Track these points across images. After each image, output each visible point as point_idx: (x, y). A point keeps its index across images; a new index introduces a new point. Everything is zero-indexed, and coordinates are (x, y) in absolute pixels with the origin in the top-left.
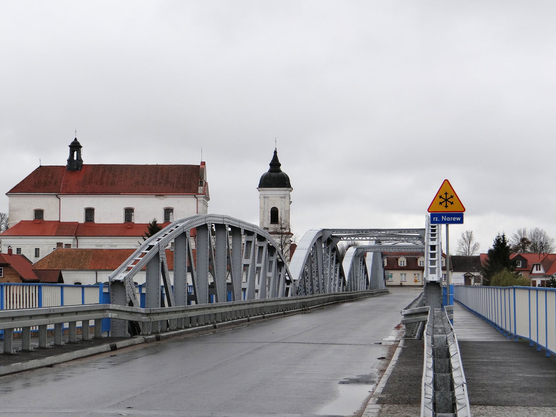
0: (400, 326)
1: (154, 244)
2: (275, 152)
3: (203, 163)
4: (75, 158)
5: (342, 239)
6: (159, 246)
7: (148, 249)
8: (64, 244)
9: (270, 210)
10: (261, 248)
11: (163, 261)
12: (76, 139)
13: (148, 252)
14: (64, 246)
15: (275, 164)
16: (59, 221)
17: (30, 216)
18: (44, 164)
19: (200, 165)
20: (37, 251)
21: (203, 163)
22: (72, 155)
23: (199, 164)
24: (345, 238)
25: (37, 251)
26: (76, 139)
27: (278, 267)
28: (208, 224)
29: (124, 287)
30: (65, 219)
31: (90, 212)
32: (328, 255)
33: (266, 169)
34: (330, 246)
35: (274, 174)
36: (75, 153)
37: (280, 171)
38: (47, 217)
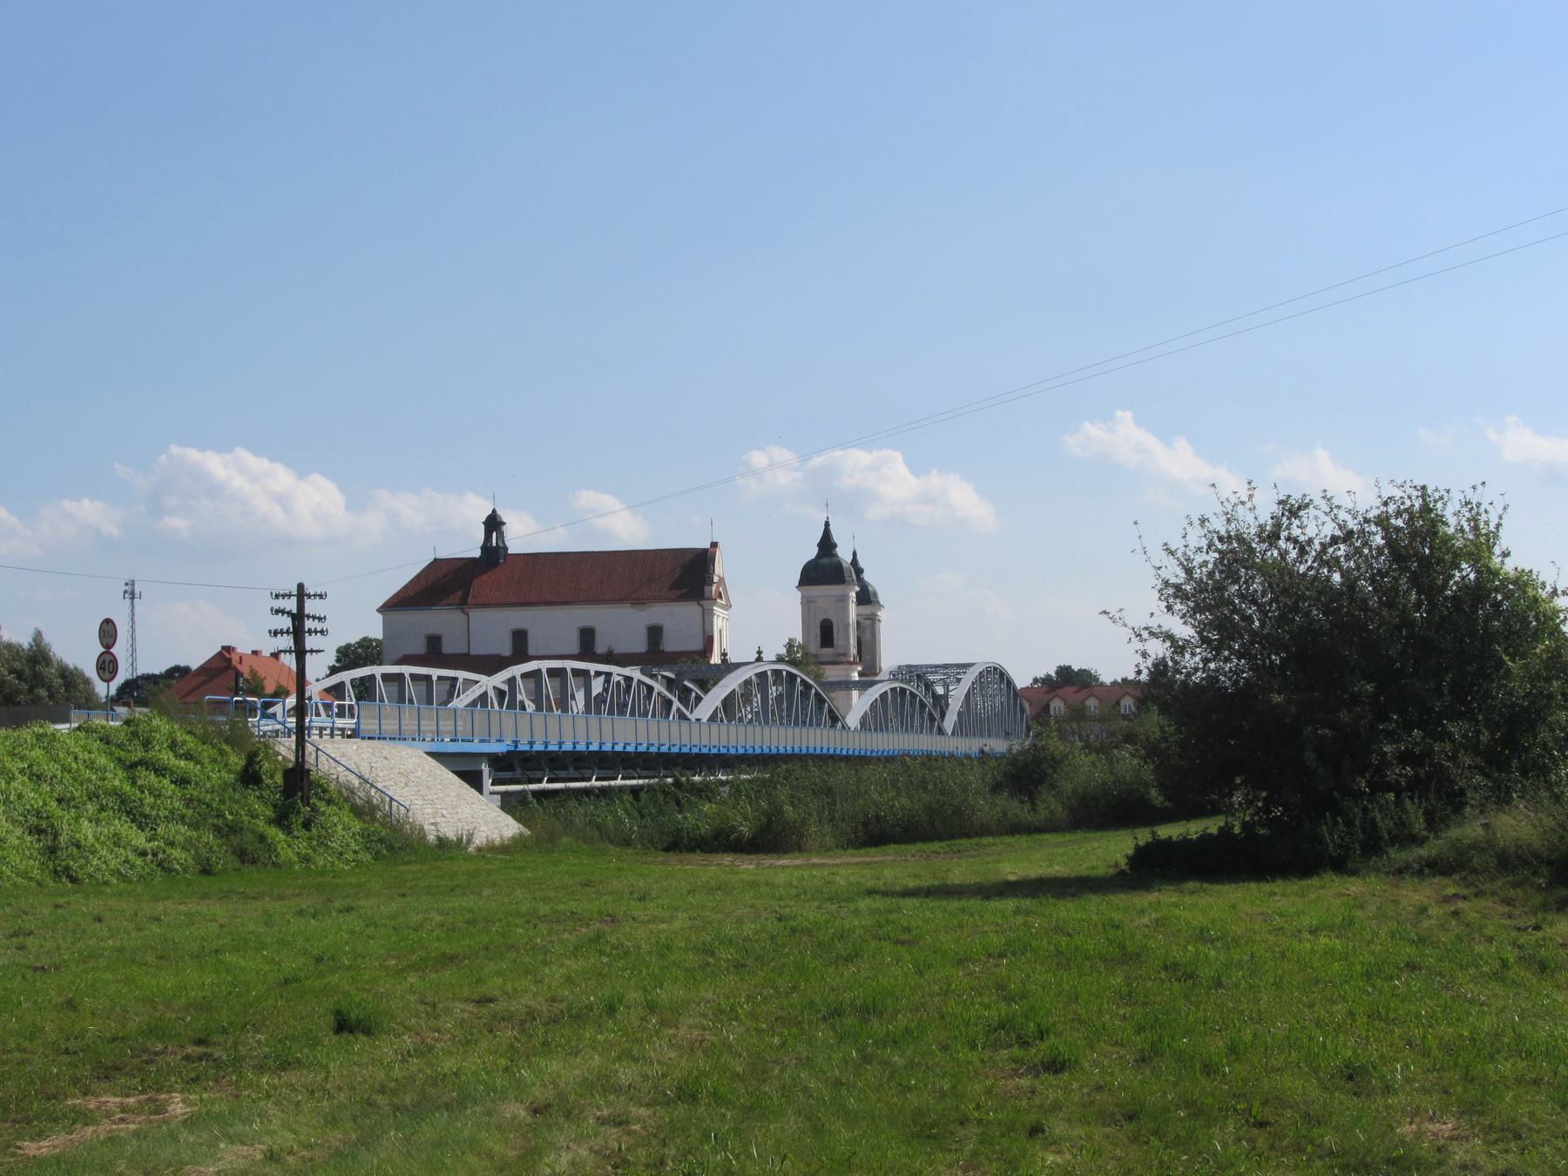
0: (1416, 938)
2: (827, 524)
3: (714, 545)
9: (818, 624)
12: (494, 511)
15: (827, 544)
18: (444, 554)
23: (708, 546)
26: (494, 511)
33: (812, 552)
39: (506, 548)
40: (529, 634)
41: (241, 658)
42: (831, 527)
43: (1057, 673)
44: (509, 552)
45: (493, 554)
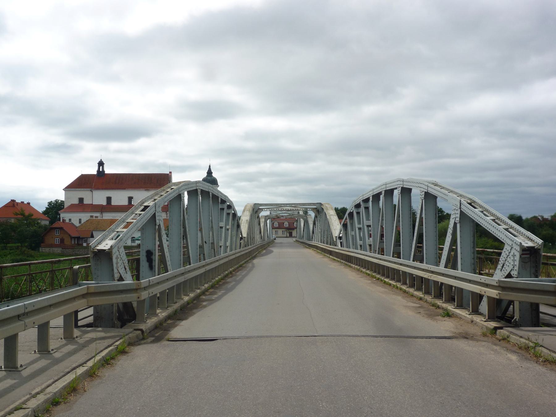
1: (149, 204)
2: (210, 166)
4: (101, 170)
5: (264, 210)
6: (155, 206)
7: (143, 210)
8: (94, 216)
10: (228, 214)
11: (160, 224)
12: (101, 160)
13: (143, 213)
14: (94, 217)
15: (210, 173)
16: (92, 204)
17: (76, 202)
19: (169, 173)
20: (80, 220)
21: (171, 173)
22: (99, 168)
24: (266, 210)
25: (80, 220)
26: (101, 160)
27: (345, 230)
28: (198, 189)
29: (111, 259)
30: (95, 203)
31: (109, 199)
32: (122, 226)
34: (256, 214)
35: (209, 178)
36: (101, 167)
37: (212, 176)
38: (86, 202)
39: (104, 172)
40: (112, 199)
41: (17, 203)
42: (211, 167)
43: (440, 208)
44: (106, 173)
45: (101, 173)
